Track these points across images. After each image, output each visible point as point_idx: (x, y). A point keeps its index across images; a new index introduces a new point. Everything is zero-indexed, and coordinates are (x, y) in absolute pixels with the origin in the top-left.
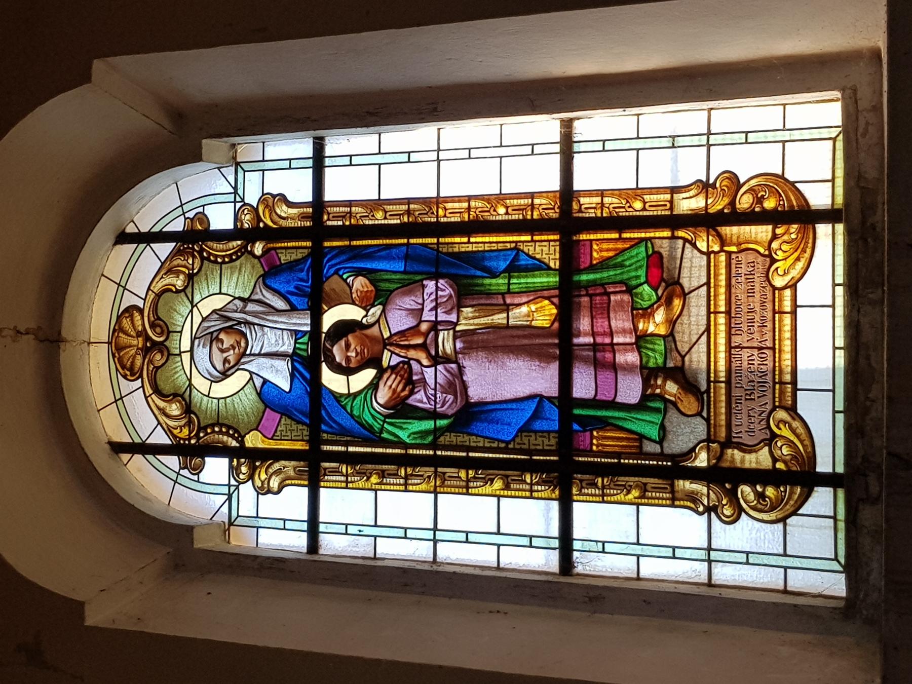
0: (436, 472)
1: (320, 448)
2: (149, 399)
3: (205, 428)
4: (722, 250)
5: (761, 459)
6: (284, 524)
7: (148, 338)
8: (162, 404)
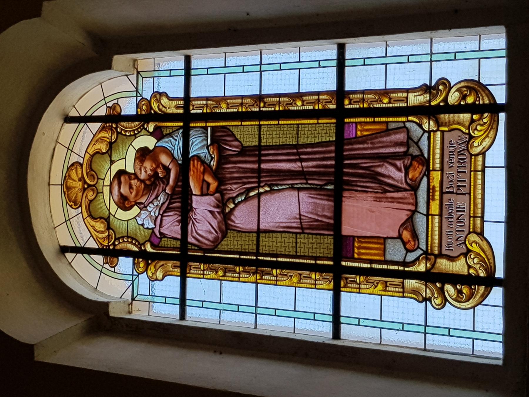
1: (334, 263)
4: (438, 130)
5: (459, 267)
6: (166, 300)
7: (85, 182)
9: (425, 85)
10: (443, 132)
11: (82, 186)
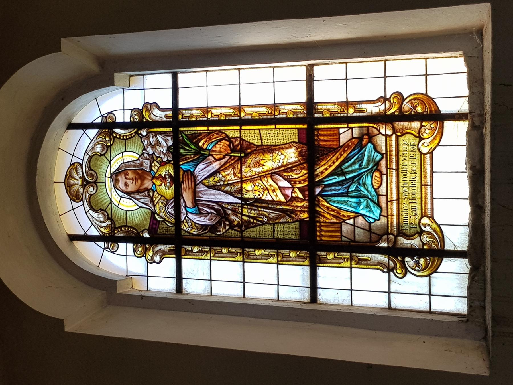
0: (278, 253)
3: (118, 228)
9: (381, 97)
10: (397, 137)
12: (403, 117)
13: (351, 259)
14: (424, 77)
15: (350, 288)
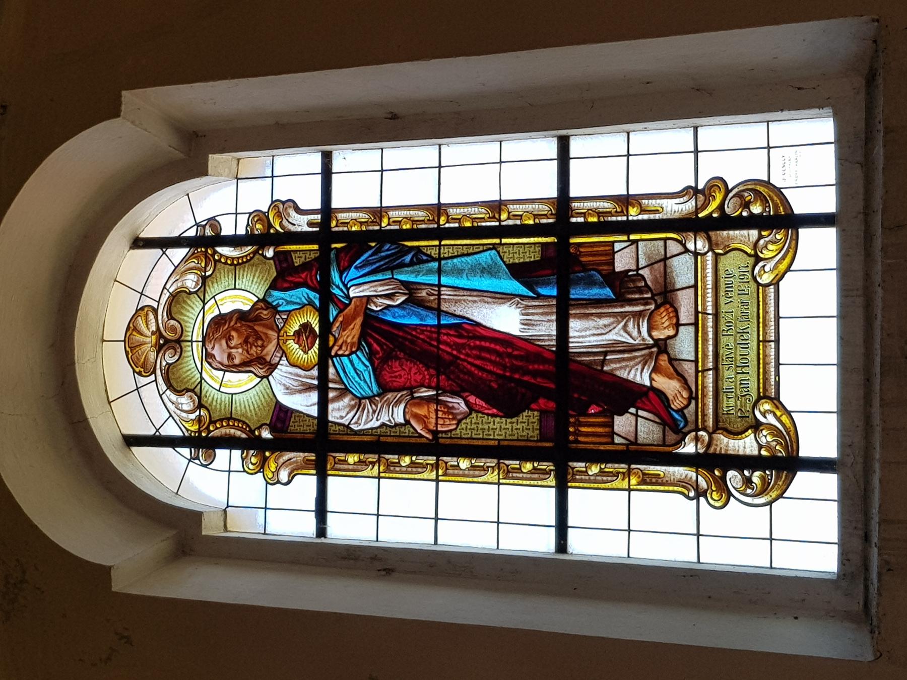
2: (164, 396)
3: (215, 422)
5: (747, 445)
8: (173, 397)
9: (690, 187)
10: (717, 255)
11: (158, 347)
12: (726, 222)
13: (436, 466)
14: (626, 158)
15: (768, 537)
